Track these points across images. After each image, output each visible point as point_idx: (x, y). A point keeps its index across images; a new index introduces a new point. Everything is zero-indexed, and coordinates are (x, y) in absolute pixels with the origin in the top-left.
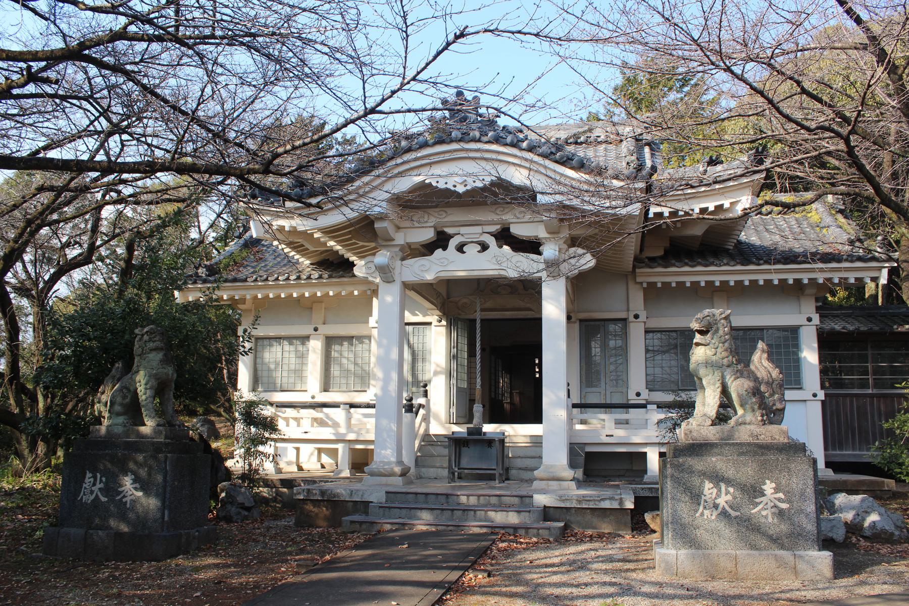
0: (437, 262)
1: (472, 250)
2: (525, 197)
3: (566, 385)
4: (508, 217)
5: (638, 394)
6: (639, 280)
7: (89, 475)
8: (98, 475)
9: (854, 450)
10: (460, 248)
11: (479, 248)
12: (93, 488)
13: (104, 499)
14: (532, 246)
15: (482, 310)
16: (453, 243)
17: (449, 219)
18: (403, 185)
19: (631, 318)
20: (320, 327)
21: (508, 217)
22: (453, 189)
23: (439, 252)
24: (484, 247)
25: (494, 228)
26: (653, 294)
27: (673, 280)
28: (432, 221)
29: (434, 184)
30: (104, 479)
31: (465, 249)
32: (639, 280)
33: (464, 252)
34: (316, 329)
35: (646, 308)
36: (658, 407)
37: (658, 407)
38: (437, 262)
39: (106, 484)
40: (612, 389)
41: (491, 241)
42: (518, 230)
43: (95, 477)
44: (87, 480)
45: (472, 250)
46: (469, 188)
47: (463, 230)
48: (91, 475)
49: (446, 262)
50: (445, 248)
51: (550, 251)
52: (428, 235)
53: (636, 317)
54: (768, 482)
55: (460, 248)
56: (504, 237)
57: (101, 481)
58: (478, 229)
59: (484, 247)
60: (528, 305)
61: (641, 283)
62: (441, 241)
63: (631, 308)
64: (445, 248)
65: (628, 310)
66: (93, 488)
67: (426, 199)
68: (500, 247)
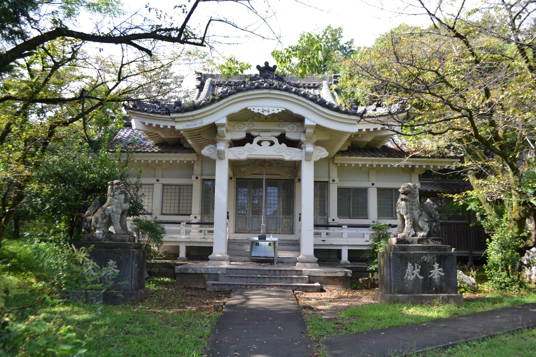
0: (248, 150)
1: (266, 144)
2: (300, 119)
3: (226, 213)
4: (286, 129)
5: (333, 220)
6: (335, 162)
7: (409, 264)
8: (416, 265)
9: (464, 250)
10: (259, 143)
11: (269, 144)
12: (414, 272)
13: (421, 277)
14: (294, 144)
15: (266, 174)
16: (256, 140)
17: (254, 127)
18: (236, 108)
19: (331, 181)
20: (160, 179)
21: (286, 129)
22: (262, 113)
23: (248, 145)
24: (272, 144)
25: (278, 134)
26: (341, 168)
27: (353, 163)
28: (246, 129)
29: (252, 110)
30: (420, 267)
31: (262, 144)
32: (335, 162)
33: (261, 146)
34: (158, 181)
35: (338, 176)
36: (348, 227)
37: (348, 227)
38: (248, 150)
39: (421, 269)
40: (320, 217)
41: (276, 141)
42: (289, 136)
43: (414, 265)
44: (409, 267)
45: (266, 144)
46: (270, 113)
47: (262, 134)
48: (411, 265)
49: (252, 150)
50: (251, 143)
51: (309, 148)
52: (241, 135)
53: (333, 181)
54: (111, 260)
55: (259, 143)
56: (282, 139)
57: (418, 268)
58: (269, 134)
59: (272, 144)
60: (278, 173)
61: (337, 164)
62: (249, 139)
63: (331, 176)
64: (251, 143)
65: (329, 177)
66: (414, 272)
67: (246, 116)
68: (280, 143)
